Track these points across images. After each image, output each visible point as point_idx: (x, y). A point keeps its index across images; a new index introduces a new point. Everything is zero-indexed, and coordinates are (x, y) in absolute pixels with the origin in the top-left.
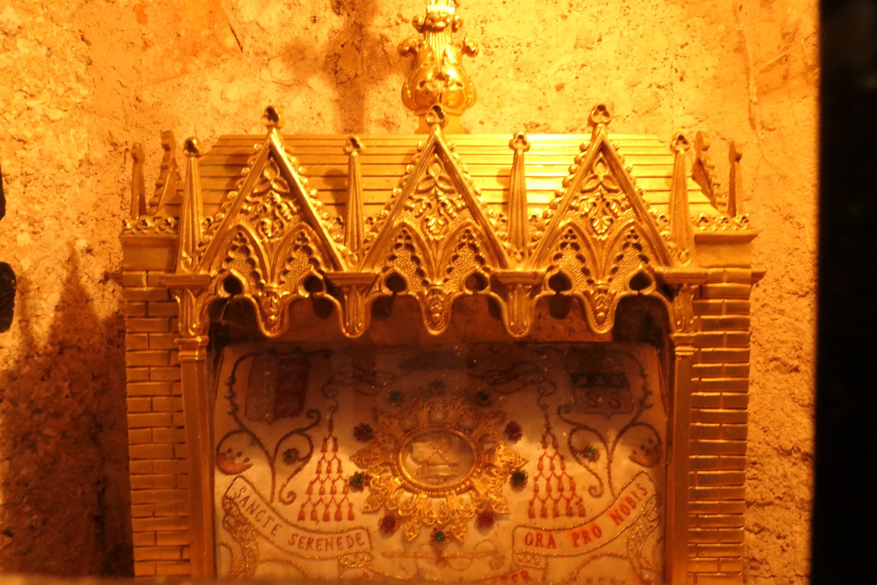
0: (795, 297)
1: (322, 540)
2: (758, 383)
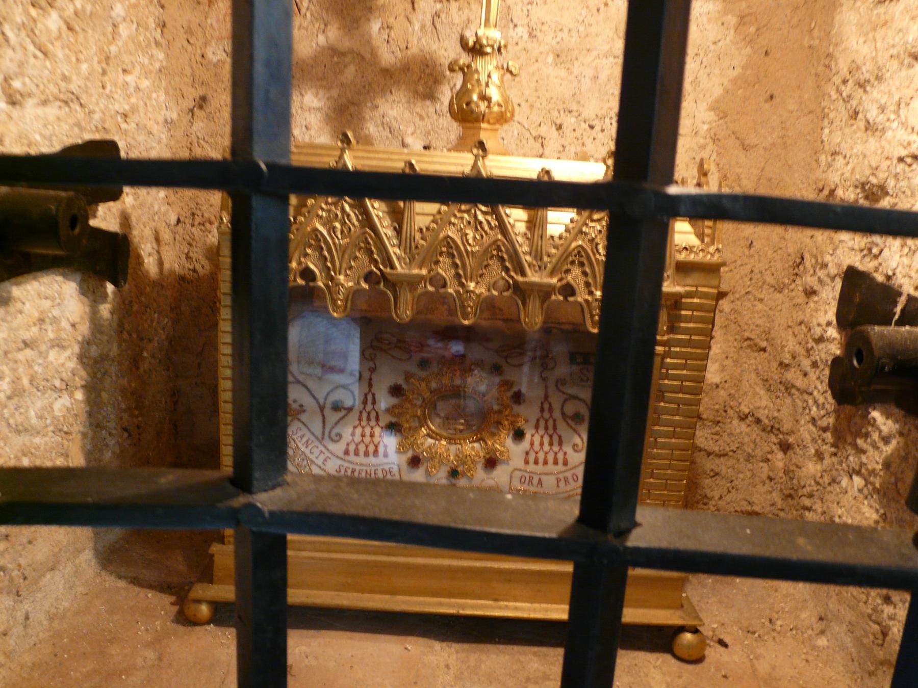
0: (772, 289)
1: (362, 470)
2: (732, 358)
